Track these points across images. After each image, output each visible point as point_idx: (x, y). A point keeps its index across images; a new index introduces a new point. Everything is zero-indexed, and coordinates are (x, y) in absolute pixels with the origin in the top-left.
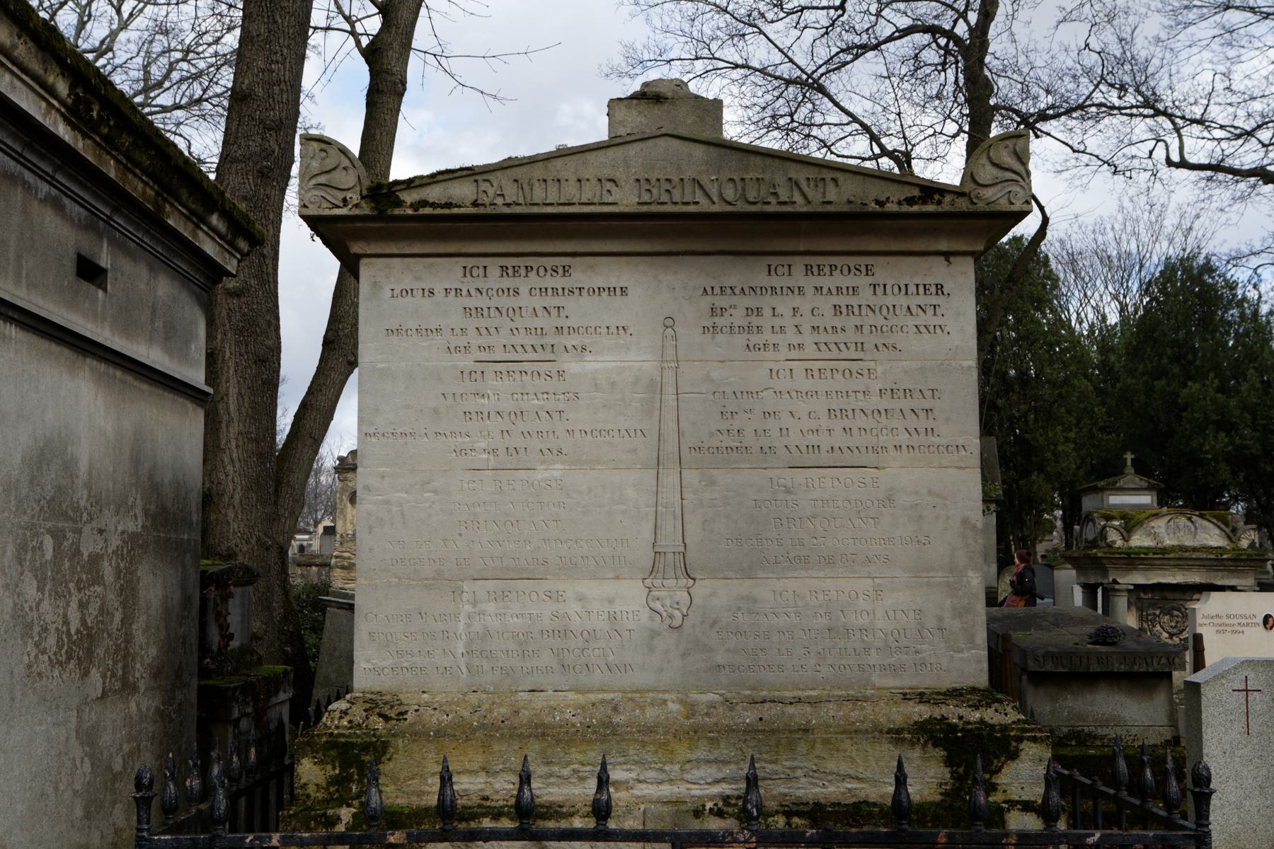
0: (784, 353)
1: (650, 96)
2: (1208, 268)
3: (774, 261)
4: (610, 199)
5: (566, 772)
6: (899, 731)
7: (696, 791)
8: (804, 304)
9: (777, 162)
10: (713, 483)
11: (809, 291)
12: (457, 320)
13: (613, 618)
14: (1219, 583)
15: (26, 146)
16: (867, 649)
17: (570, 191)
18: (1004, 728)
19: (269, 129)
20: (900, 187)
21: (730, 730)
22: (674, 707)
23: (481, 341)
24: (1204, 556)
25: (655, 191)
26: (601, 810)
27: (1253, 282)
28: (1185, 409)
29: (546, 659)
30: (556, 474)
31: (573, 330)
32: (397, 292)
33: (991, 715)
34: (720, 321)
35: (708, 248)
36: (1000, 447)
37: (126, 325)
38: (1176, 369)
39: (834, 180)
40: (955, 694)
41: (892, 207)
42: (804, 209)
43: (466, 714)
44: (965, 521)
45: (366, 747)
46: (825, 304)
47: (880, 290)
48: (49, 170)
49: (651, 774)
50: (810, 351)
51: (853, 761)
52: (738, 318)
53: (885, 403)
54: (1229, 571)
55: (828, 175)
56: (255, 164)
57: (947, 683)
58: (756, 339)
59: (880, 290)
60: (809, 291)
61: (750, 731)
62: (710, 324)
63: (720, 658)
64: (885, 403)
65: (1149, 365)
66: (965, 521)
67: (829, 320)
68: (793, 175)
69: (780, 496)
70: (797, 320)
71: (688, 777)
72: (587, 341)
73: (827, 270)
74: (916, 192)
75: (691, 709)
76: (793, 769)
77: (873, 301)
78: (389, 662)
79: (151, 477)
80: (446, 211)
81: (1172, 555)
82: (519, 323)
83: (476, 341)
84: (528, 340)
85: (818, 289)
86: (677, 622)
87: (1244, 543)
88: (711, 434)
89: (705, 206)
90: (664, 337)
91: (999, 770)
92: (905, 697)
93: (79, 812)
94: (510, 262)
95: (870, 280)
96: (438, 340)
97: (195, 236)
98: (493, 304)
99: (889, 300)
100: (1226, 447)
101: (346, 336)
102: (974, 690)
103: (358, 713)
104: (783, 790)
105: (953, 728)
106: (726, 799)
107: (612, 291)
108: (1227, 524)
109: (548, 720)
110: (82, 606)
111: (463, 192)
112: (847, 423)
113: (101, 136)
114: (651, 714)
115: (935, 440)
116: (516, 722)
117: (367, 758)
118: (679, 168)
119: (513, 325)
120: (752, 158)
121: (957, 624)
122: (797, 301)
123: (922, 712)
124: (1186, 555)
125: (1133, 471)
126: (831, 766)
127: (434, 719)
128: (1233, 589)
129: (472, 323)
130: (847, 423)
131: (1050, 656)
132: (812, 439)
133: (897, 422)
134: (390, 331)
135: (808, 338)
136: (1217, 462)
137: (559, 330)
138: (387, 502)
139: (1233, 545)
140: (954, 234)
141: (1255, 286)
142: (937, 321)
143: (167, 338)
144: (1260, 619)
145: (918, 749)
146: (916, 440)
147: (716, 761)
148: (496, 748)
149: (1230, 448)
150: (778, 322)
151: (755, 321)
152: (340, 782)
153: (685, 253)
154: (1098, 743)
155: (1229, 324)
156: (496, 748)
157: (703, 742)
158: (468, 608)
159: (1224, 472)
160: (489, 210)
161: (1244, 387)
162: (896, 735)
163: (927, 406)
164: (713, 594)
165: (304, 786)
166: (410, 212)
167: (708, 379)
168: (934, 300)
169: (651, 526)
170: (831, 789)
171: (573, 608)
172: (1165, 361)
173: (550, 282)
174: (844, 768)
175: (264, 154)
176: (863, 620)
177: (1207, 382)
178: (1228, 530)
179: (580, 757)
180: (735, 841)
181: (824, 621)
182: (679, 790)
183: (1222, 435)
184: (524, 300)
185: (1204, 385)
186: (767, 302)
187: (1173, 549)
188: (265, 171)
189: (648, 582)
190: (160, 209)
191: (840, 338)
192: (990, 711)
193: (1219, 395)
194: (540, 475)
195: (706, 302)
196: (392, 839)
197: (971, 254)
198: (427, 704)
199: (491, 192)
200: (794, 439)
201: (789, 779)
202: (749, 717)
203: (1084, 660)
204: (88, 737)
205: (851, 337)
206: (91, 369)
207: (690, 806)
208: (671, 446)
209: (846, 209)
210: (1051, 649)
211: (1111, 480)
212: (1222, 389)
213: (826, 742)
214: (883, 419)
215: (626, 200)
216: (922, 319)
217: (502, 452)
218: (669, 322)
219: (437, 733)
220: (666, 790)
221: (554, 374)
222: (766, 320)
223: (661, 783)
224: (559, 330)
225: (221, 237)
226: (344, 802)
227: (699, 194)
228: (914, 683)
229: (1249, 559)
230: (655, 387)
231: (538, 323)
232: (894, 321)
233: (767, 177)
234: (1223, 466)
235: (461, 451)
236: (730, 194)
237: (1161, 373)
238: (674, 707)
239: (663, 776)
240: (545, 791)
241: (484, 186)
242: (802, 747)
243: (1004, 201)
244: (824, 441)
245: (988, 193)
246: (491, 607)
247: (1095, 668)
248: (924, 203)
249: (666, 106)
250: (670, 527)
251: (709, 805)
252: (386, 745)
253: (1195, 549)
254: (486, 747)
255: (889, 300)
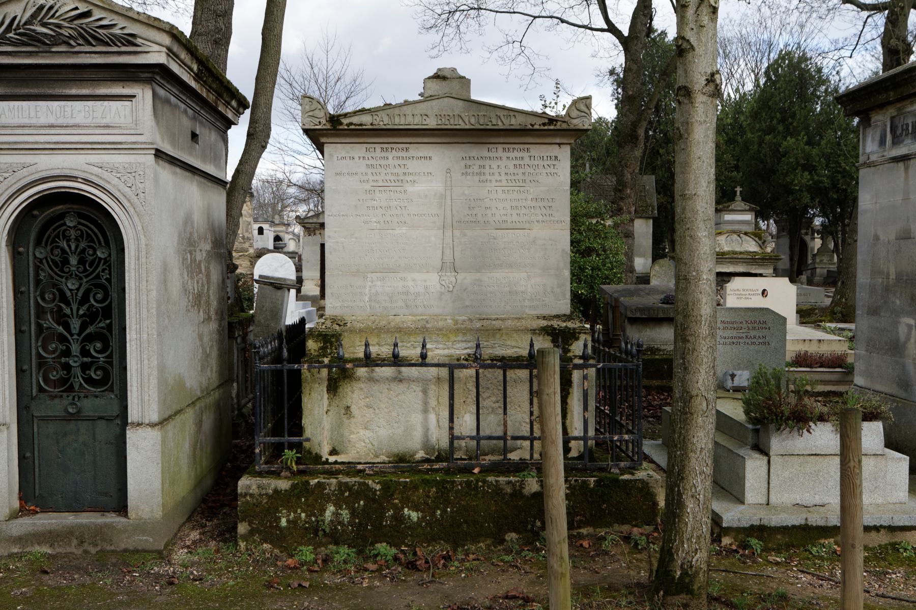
0: (494, 183)
1: (439, 77)
2: (804, 58)
3: (491, 146)
4: (425, 123)
5: (409, 345)
6: (535, 330)
7: (458, 352)
8: (502, 164)
9: (492, 108)
10: (465, 235)
11: (504, 158)
12: (363, 169)
13: (426, 288)
14: (754, 272)
15: (181, 92)
16: (524, 300)
17: (410, 119)
18: (574, 329)
19: (219, 16)
20: (540, 119)
21: (471, 330)
22: (449, 321)
23: (374, 178)
24: (745, 257)
25: (443, 120)
26: (424, 356)
27: (837, 69)
28: (784, 156)
29: (400, 303)
30: (404, 231)
31: (411, 174)
32: (339, 158)
33: (570, 324)
34: (469, 171)
35: (464, 141)
36: (656, 181)
37: (204, 159)
38: (781, 128)
39: (514, 116)
40: (557, 317)
41: (536, 127)
42: (502, 128)
43: (370, 324)
44: (563, 250)
45: (333, 336)
46: (511, 164)
47: (532, 158)
48: (184, 98)
49: (441, 346)
50: (504, 183)
51: (517, 341)
52: (476, 169)
53: (533, 204)
54: (759, 265)
55: (512, 113)
56: (212, 36)
57: (554, 313)
58: (482, 178)
59: (532, 158)
60: (504, 158)
61: (478, 330)
62: (464, 172)
63: (467, 303)
64: (533, 204)
65: (764, 125)
66: (563, 250)
67: (512, 170)
68: (498, 114)
69: (492, 240)
70: (499, 170)
71: (455, 347)
72: (416, 178)
73: (511, 150)
74: (547, 121)
75: (456, 322)
76: (494, 344)
77: (530, 163)
78: (339, 304)
79: (212, 224)
80: (360, 127)
81: (727, 256)
82: (389, 171)
83: (371, 178)
84: (392, 178)
85: (508, 158)
86: (451, 289)
87: (769, 250)
88: (465, 216)
89: (463, 126)
90: (446, 177)
91: (571, 344)
92: (538, 318)
93: (199, 369)
94: (386, 146)
95: (529, 154)
96: (356, 177)
97: (226, 111)
98: (378, 163)
99: (536, 163)
100: (808, 181)
101: (260, 131)
102: (565, 315)
103: (328, 323)
104: (491, 351)
105: (555, 329)
106: (469, 355)
107: (426, 158)
108: (760, 239)
109: (401, 326)
110: (198, 282)
111: (366, 119)
112: (518, 212)
113: (203, 81)
114: (441, 324)
115: (553, 218)
116: (389, 326)
117: (334, 340)
118: (453, 110)
119: (385, 172)
120: (482, 106)
121: (559, 290)
122: (499, 163)
123: (544, 323)
124: (735, 256)
125: (740, 199)
126: (509, 343)
127: (358, 326)
128: (761, 275)
129: (369, 171)
130: (518, 212)
131: (638, 309)
132: (504, 218)
133: (538, 211)
134: (337, 174)
135: (504, 178)
136: (802, 191)
137: (405, 174)
138: (337, 242)
139: (762, 251)
140: (562, 136)
141: (838, 73)
142: (555, 171)
143: (215, 160)
144: (760, 292)
145: (541, 336)
146: (545, 218)
147: (465, 341)
148: (382, 336)
149: (811, 182)
150: (492, 171)
151: (483, 170)
152: (323, 348)
153: (455, 143)
154: (661, 353)
155: (819, 97)
156: (382, 336)
157: (460, 334)
158: (370, 283)
159: (806, 198)
160: (377, 127)
161: (823, 142)
162: (533, 331)
163: (550, 205)
164: (465, 279)
165: (310, 350)
166: (346, 127)
167: (463, 194)
168: (554, 162)
169: (441, 252)
170: (509, 351)
171: (410, 283)
172: (775, 122)
173: (401, 154)
174: (514, 344)
175: (217, 30)
176: (523, 289)
177: (800, 138)
178: (760, 242)
179: (414, 340)
180: (472, 367)
181: (508, 289)
182: (452, 351)
183: (806, 173)
184: (391, 161)
185: (797, 140)
186: (487, 163)
187: (728, 253)
188: (218, 40)
189: (440, 274)
190: (216, 103)
191: (516, 177)
192: (570, 323)
193: (807, 147)
194: (397, 232)
195: (464, 162)
196: (348, 366)
197: (569, 144)
198: (355, 320)
199: (378, 119)
200: (497, 218)
201: (492, 348)
202: (478, 325)
203: (656, 312)
204: (201, 337)
205: (521, 177)
206: (197, 180)
207: (456, 357)
208: (449, 221)
209: (518, 127)
210: (640, 306)
211: (726, 205)
212: (808, 143)
213: (507, 334)
214: (532, 210)
215: (432, 123)
216: (549, 170)
217: (382, 223)
218: (448, 171)
219: (360, 330)
220: (446, 352)
221: (403, 191)
222: (487, 170)
223: (444, 349)
224: (405, 174)
225: (234, 109)
226: (325, 356)
227: (461, 121)
228: (542, 313)
229: (770, 259)
230: (443, 197)
231: (396, 171)
232: (537, 171)
233: (488, 114)
234: (805, 194)
235: (366, 222)
236: (473, 121)
237: (771, 130)
238: (449, 321)
239: (445, 347)
240: (403, 353)
241: (375, 117)
242: (498, 336)
243: (581, 125)
244: (509, 219)
245: (575, 121)
246: (379, 283)
247: (661, 315)
248: (550, 125)
249: (448, 82)
250: (448, 252)
251: (462, 357)
252: (340, 335)
253: (741, 253)
254: (378, 336)
255: (536, 163)
